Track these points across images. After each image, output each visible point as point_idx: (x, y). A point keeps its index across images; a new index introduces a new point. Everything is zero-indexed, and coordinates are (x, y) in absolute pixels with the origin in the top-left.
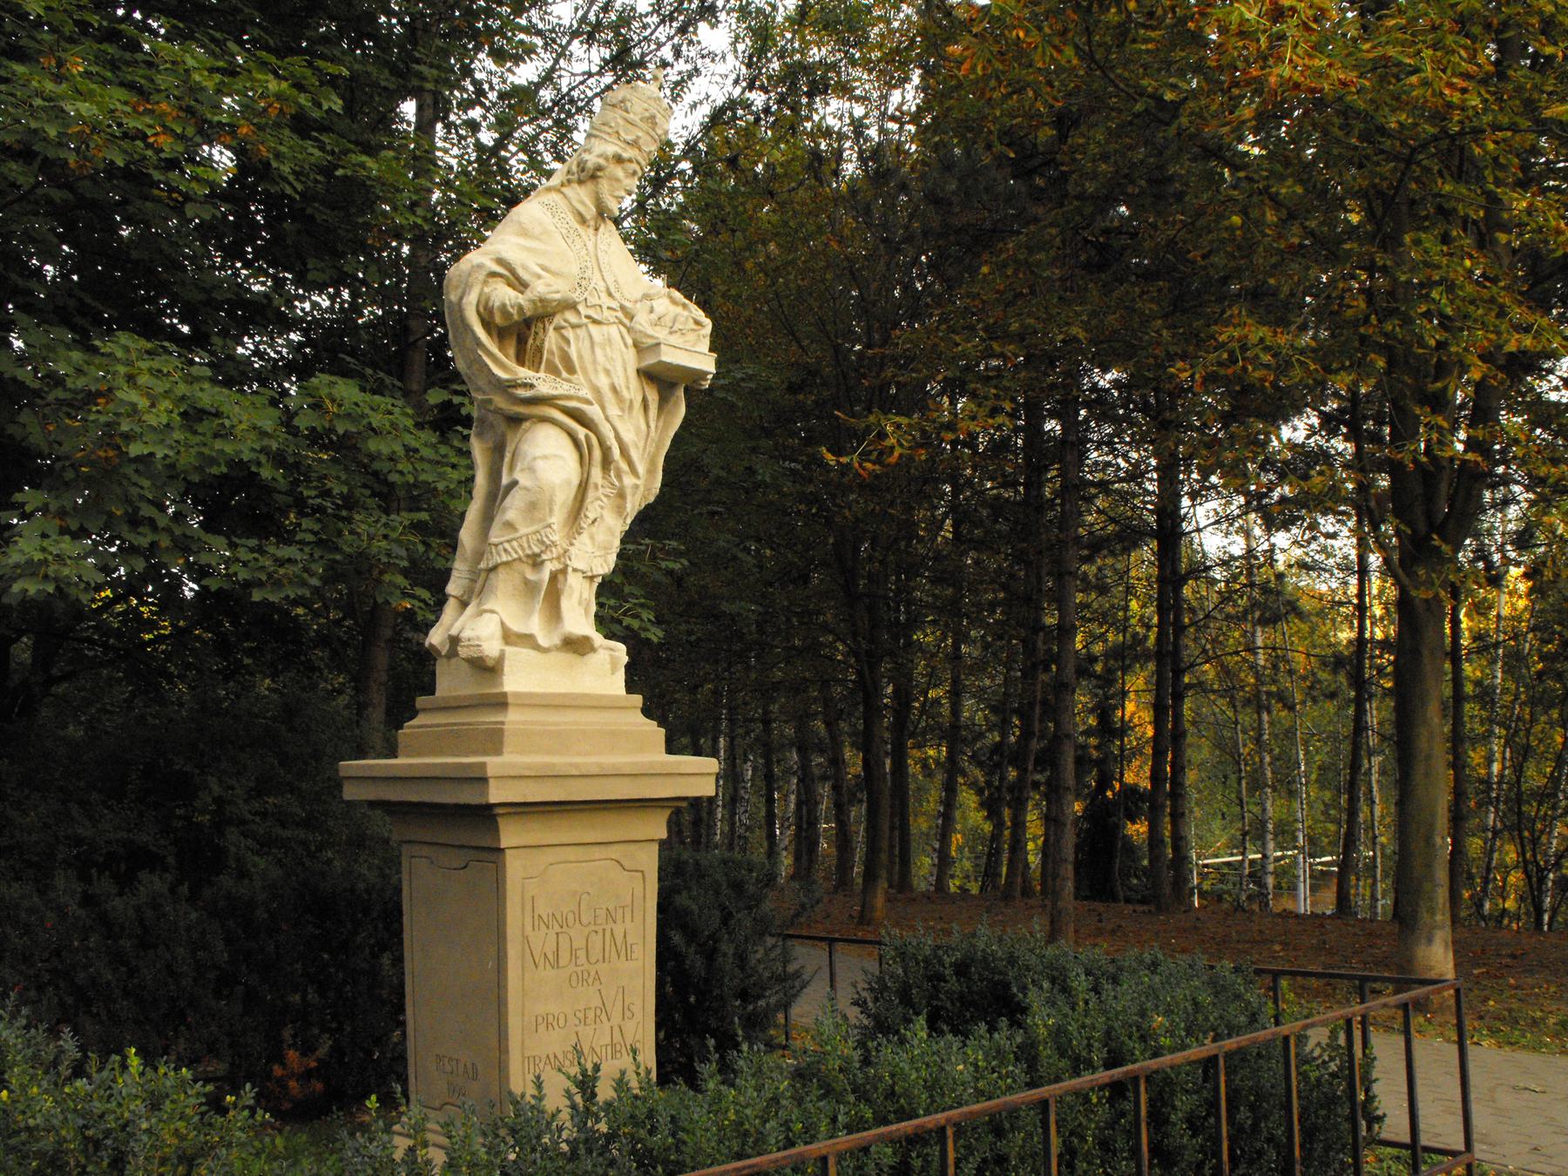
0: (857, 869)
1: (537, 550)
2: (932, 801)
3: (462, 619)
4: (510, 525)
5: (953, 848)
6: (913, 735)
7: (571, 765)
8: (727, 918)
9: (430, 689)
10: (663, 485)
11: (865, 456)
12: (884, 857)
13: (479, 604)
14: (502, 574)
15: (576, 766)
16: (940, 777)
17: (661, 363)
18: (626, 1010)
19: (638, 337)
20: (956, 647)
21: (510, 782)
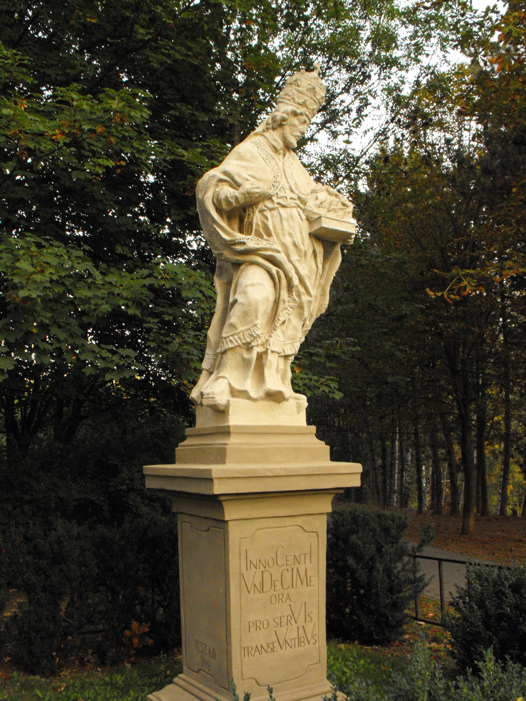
0: (461, 506)
1: (248, 340)
2: (498, 469)
3: (209, 381)
4: (233, 326)
5: (509, 491)
6: (487, 439)
7: (266, 470)
8: (379, 550)
9: (192, 423)
10: (330, 301)
11: (451, 291)
12: (474, 501)
13: (218, 373)
14: (229, 355)
15: (271, 470)
16: (501, 458)
17: (322, 228)
18: (307, 617)
19: (309, 213)
20: (507, 395)
21: (228, 481)
